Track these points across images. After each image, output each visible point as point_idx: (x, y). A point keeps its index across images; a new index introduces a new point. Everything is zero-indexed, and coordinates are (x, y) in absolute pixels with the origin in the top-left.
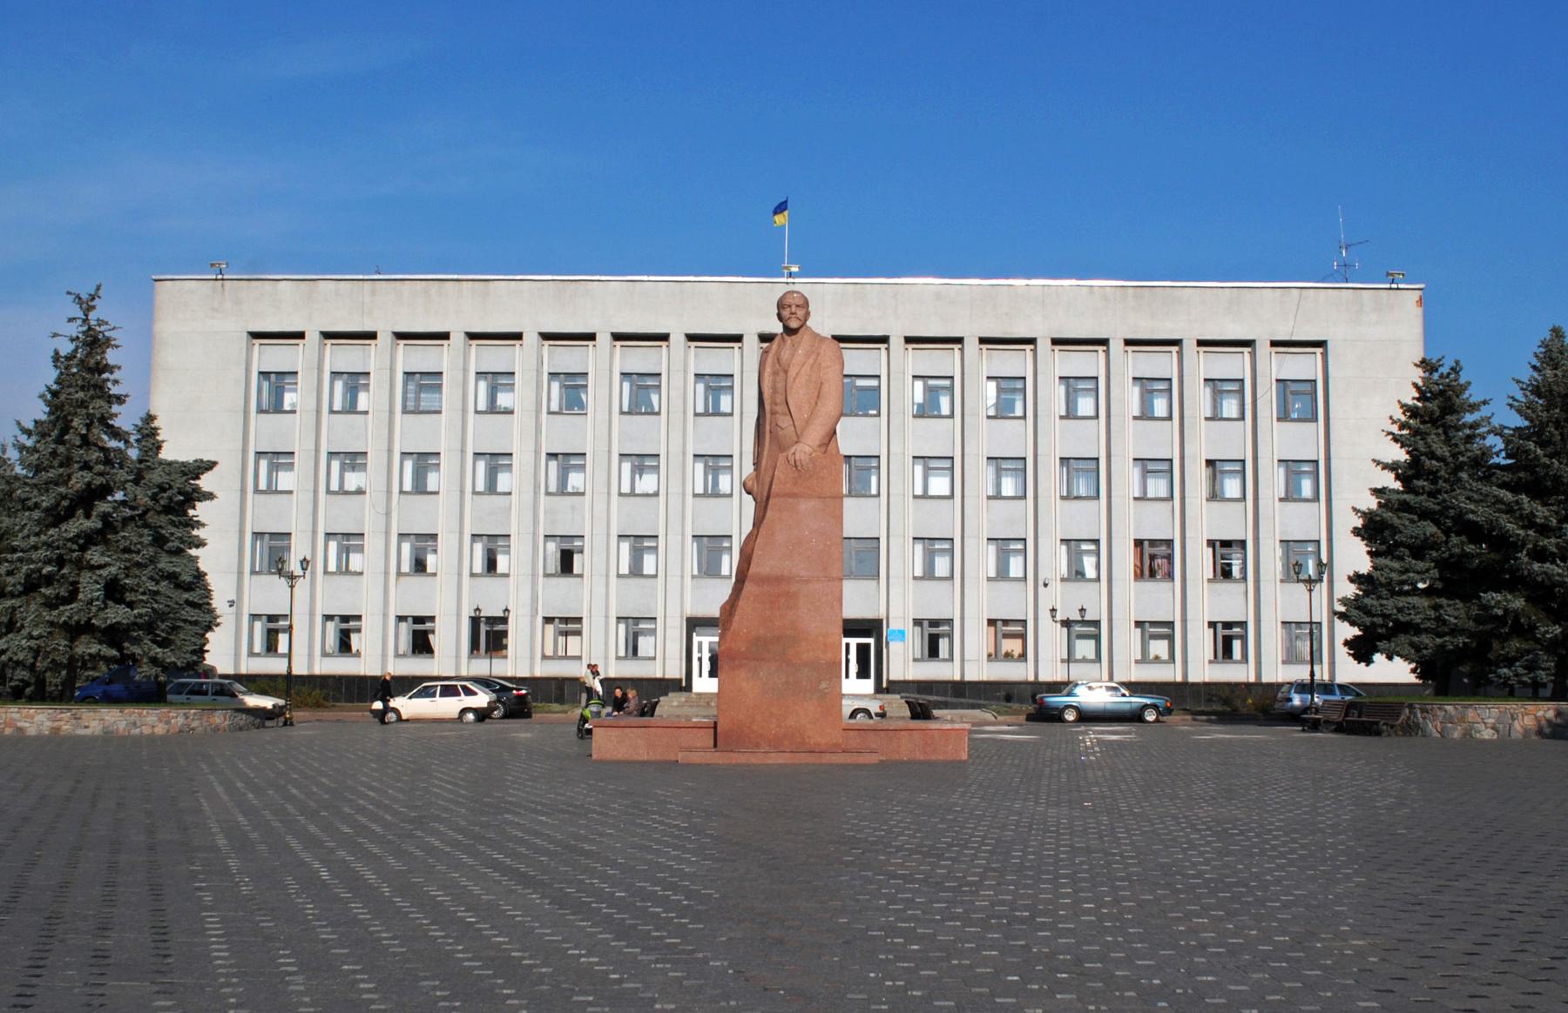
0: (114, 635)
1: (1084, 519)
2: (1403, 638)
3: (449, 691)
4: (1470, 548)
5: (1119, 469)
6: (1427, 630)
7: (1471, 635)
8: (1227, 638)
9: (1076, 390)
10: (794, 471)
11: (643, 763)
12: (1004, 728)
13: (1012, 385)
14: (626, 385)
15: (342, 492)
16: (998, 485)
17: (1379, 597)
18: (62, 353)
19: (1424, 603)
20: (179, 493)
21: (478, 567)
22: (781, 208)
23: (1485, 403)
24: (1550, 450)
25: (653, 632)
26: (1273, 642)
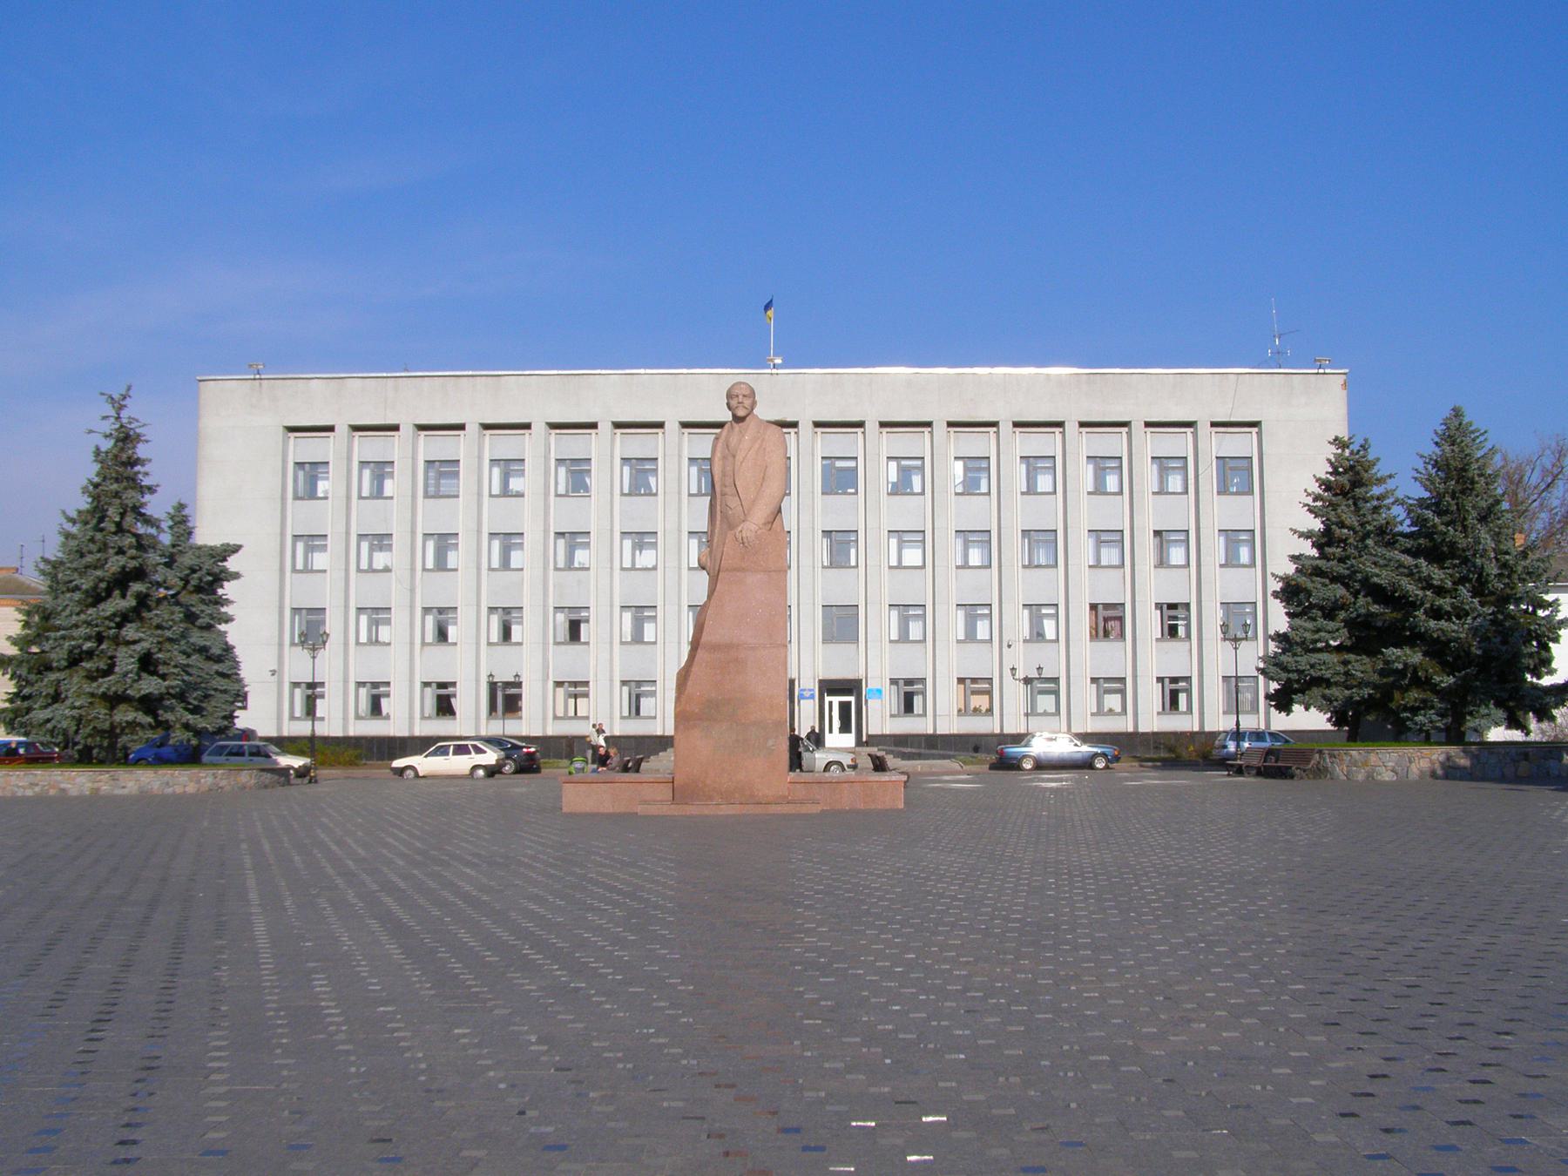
0: (149, 704)
1: (1045, 586)
2: (1316, 691)
3: (461, 750)
4: (1375, 608)
5: (1052, 537)
6: (1336, 684)
7: (1375, 687)
8: (1174, 692)
9: (1036, 469)
10: (739, 548)
11: (609, 816)
12: (956, 776)
13: (976, 464)
14: (626, 469)
15: (371, 570)
16: (966, 556)
17: (1295, 655)
18: (103, 449)
19: (1333, 658)
20: (207, 577)
21: (495, 636)
22: (767, 307)
23: (1390, 476)
24: (1447, 518)
25: (653, 694)
26: (1215, 696)
